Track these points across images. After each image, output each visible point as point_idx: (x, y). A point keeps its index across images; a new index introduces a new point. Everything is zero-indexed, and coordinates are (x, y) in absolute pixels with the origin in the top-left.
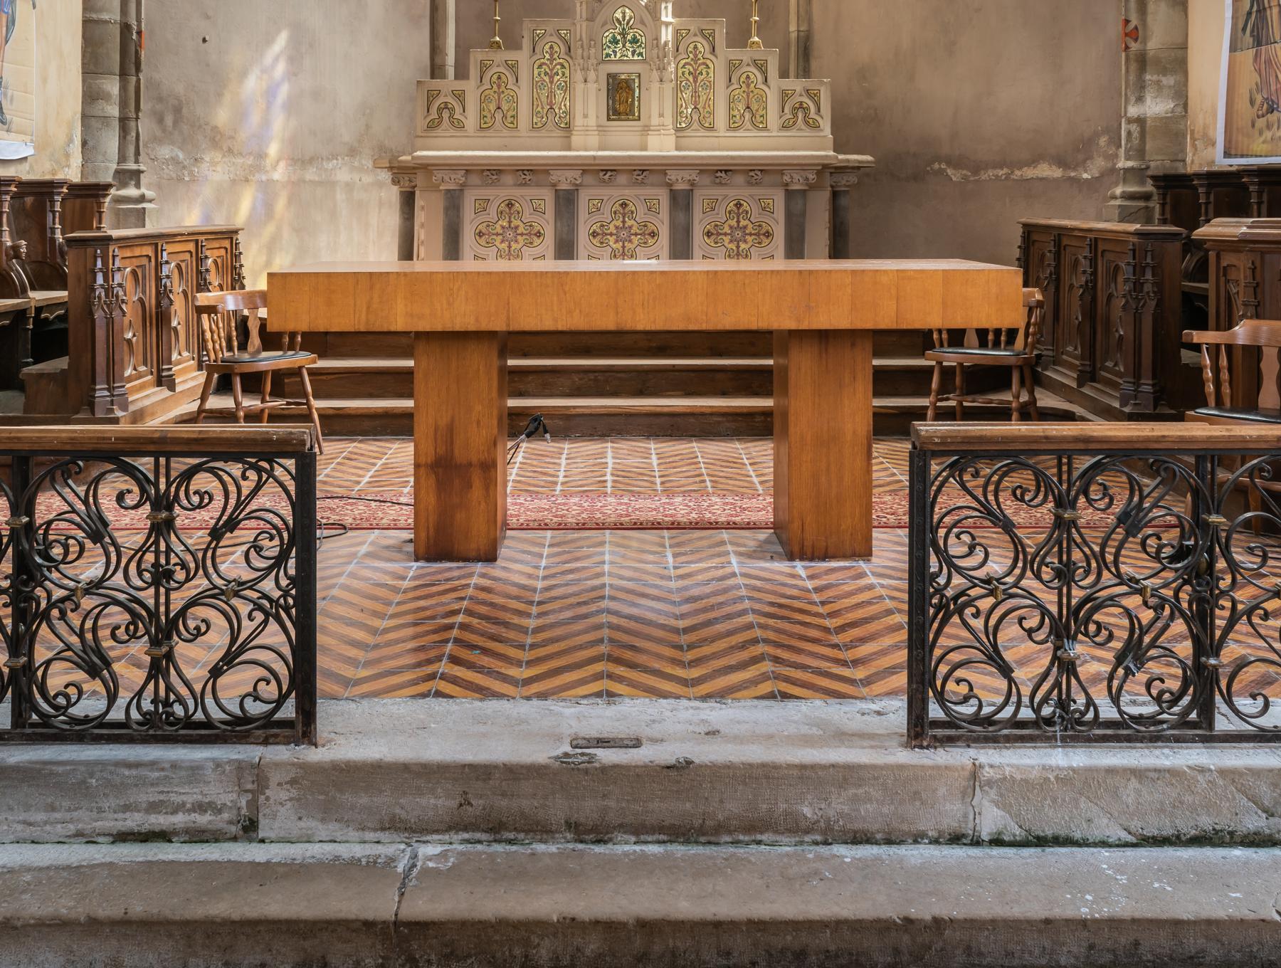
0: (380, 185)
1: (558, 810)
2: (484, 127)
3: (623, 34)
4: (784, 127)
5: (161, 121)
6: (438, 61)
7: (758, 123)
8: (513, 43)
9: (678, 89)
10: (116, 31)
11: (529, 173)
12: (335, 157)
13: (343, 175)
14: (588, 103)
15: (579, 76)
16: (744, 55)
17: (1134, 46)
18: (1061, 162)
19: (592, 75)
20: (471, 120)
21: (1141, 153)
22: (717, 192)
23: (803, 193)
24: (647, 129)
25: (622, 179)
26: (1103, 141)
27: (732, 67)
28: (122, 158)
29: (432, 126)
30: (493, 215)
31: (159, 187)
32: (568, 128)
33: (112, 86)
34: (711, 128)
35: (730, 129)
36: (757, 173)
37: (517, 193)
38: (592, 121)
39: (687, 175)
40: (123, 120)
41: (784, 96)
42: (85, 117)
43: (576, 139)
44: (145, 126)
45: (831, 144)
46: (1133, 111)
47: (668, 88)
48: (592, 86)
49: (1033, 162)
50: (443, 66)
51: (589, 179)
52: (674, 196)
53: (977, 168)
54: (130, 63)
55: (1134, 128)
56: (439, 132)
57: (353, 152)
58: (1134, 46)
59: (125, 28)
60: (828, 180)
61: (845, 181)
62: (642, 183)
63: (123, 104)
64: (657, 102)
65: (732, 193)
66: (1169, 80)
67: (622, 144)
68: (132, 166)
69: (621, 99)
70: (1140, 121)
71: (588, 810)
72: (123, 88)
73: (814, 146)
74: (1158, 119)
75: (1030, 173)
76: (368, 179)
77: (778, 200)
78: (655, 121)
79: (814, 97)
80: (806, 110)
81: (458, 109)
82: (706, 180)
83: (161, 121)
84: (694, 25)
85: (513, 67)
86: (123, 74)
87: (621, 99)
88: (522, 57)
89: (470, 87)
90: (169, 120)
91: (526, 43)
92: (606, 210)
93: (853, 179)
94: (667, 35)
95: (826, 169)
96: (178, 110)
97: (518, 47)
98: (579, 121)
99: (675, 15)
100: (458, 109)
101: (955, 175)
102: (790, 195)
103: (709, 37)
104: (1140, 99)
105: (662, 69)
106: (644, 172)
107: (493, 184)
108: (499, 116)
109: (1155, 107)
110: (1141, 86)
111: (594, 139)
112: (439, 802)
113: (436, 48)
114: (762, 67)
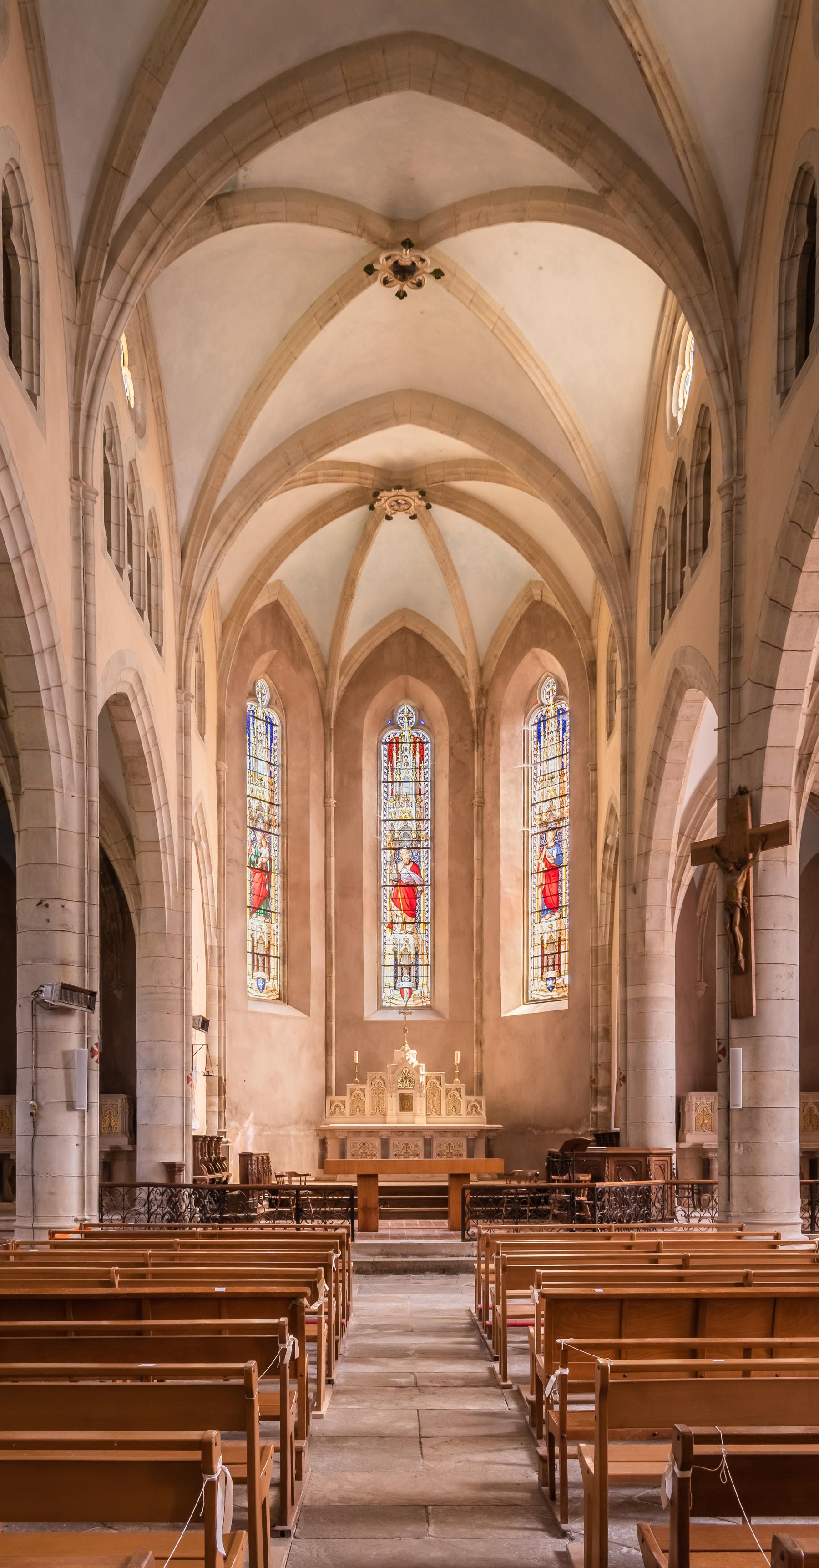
0: (307, 1136)
1: (399, 1252)
2: (352, 1114)
3: (406, 1078)
4: (468, 1114)
5: (231, 1112)
6: (328, 1084)
7: (458, 1113)
8: (363, 1082)
9: (427, 1099)
10: (217, 1079)
11: (371, 1132)
12: (290, 1125)
13: (293, 1132)
14: (393, 1104)
15: (389, 1095)
16: (452, 1086)
17: (594, 1086)
18: (572, 1128)
19: (394, 1094)
20: (347, 1111)
21: (596, 1125)
22: (442, 1139)
23: (473, 1139)
24: (415, 1115)
25: (406, 1134)
26: (585, 1120)
27: (448, 1091)
28: (220, 1127)
29: (333, 1113)
30: (401, 1148)
31: (231, 1138)
32: (385, 1114)
33: (216, 1100)
34: (440, 1114)
35: (447, 1115)
36: (456, 1132)
37: (367, 1139)
38: (394, 1112)
39: (432, 1133)
40: (220, 1113)
41: (468, 1102)
42: (207, 1112)
43: (388, 1119)
44: (227, 1114)
45: (485, 1121)
46: (593, 1110)
47: (424, 1099)
48: (394, 1099)
49: (562, 1128)
50: (330, 1087)
51: (394, 1134)
52: (425, 1140)
53: (543, 1129)
54: (222, 1091)
55: (594, 1116)
56: (335, 1116)
57: (297, 1123)
58: (594, 1086)
59: (220, 1078)
60: (485, 1135)
61: (492, 1135)
62: (414, 1136)
63: (220, 1107)
64: (419, 1104)
65: (447, 1139)
66: (605, 1099)
67: (407, 1120)
68: (223, 1130)
69: (406, 1103)
70: (596, 1113)
71: (404, 1251)
72: (220, 1101)
73: (479, 1121)
74: (602, 1113)
75: (562, 1132)
76: (302, 1134)
77: (464, 1142)
78: (418, 1112)
79: (479, 1102)
80: (476, 1108)
81: (342, 1107)
82: (437, 1135)
83: (231, 1112)
84: (432, 1074)
85: (363, 1091)
86: (220, 1095)
87: (406, 1103)
88: (367, 1087)
89: (347, 1099)
90: (234, 1112)
91: (368, 1081)
92: (358, 1146)
93: (495, 1134)
94: (422, 1079)
95: (481, 1131)
96: (236, 1108)
97: (365, 1083)
98: (389, 1112)
99: (426, 1070)
100: (342, 1107)
101: (536, 1132)
102: (468, 1140)
103: (439, 1079)
104: (596, 1105)
105: (421, 1092)
106: (415, 1132)
107: (358, 1136)
108: (358, 1110)
109: (601, 1108)
110: (596, 1101)
111: (395, 1119)
112: (378, 1250)
113: (327, 1079)
114: (459, 1091)
